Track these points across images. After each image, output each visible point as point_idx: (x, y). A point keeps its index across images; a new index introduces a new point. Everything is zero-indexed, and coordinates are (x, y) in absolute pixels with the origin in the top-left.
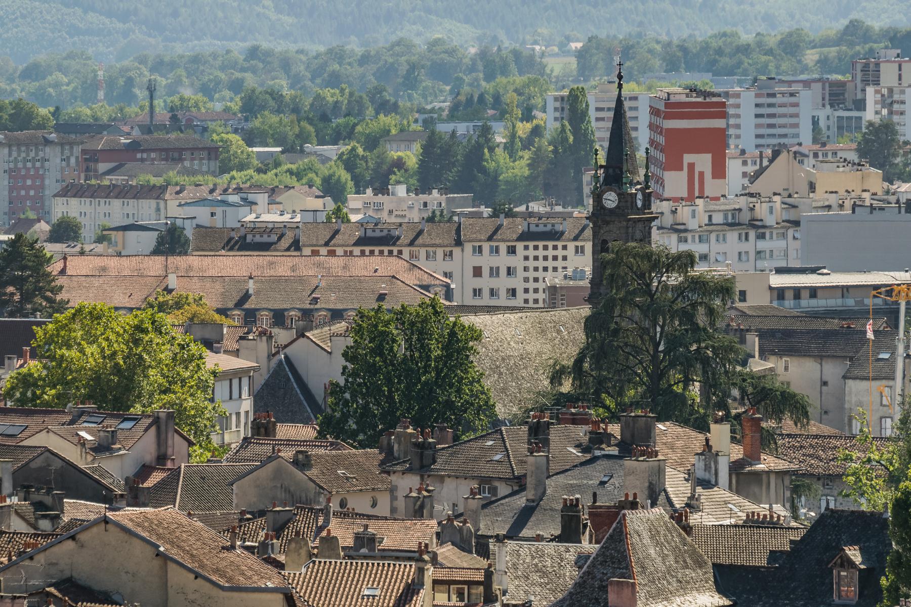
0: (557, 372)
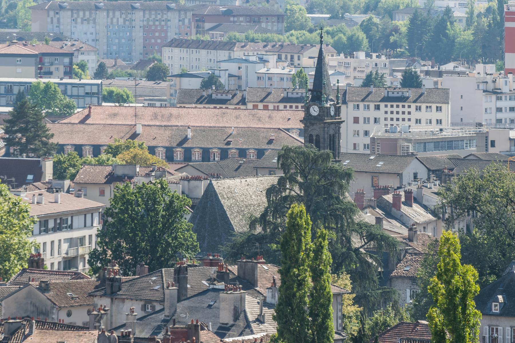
0: (253, 221)
